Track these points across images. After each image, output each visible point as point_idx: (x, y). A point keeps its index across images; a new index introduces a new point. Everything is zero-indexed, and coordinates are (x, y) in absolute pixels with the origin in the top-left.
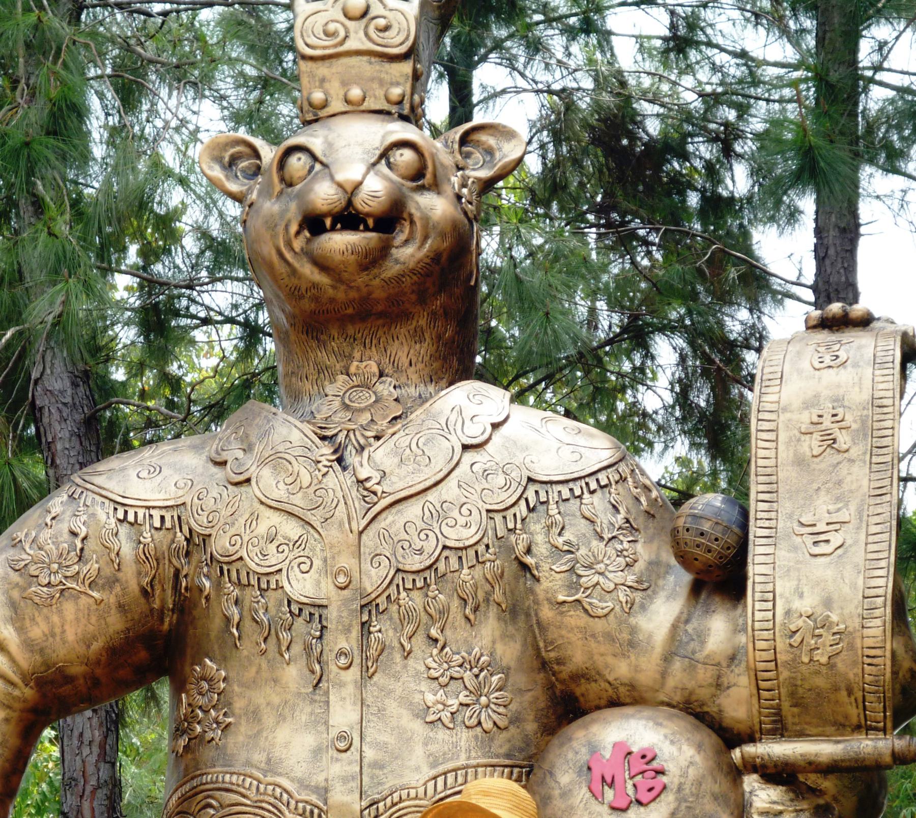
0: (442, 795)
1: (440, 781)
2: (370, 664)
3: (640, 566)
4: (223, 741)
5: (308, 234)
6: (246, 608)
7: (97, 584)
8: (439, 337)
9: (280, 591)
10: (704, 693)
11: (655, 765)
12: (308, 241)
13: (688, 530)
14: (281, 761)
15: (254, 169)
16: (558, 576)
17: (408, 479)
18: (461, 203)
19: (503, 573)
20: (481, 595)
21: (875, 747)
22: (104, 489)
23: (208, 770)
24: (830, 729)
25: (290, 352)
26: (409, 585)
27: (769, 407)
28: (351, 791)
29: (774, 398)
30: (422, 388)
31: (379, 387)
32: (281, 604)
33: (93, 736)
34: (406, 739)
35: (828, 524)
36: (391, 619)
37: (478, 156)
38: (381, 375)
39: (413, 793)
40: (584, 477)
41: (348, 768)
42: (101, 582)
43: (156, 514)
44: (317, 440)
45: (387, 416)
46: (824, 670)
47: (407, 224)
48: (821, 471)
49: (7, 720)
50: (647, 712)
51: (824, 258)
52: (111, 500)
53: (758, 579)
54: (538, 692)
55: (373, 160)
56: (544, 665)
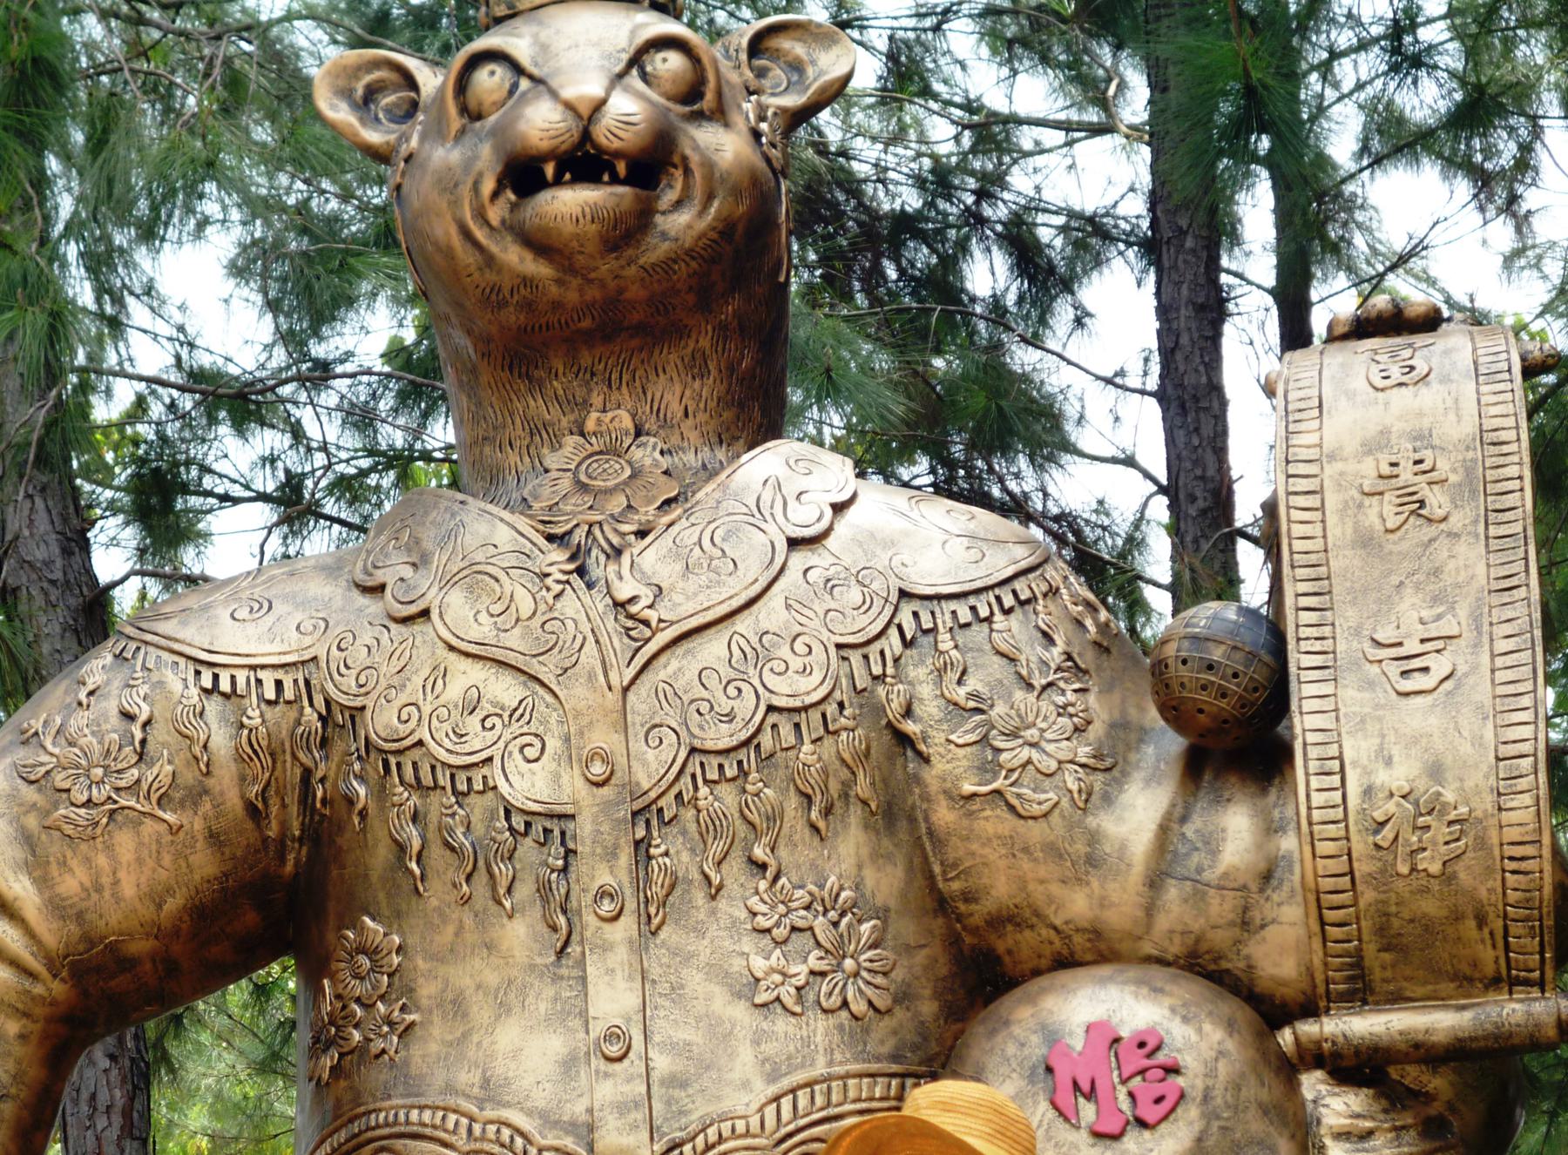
0: (791, 1127)
1: (786, 1103)
2: (652, 910)
3: (1096, 730)
4: (403, 1053)
5: (512, 197)
6: (432, 827)
7: (171, 800)
8: (731, 368)
9: (490, 794)
10: (1220, 938)
11: (1161, 1057)
12: (514, 207)
13: (1184, 662)
14: (507, 1082)
15: (405, 107)
16: (961, 752)
17: (701, 597)
18: (761, 145)
19: (868, 748)
20: (834, 788)
21: (1529, 1014)
22: (176, 640)
23: (378, 1105)
24: (1447, 987)
25: (479, 404)
26: (713, 775)
27: (1304, 454)
28: (634, 1127)
29: (1312, 439)
30: (706, 453)
31: (637, 454)
32: (493, 816)
33: (112, 1097)
34: (721, 1035)
35: (1422, 641)
36: (684, 833)
37: (778, 74)
38: (638, 434)
39: (740, 1126)
40: (992, 587)
41: (626, 1088)
42: (177, 795)
43: (268, 678)
44: (542, 541)
45: (654, 498)
46: (1435, 885)
47: (678, 173)
48: (1404, 556)
49: (22, 1037)
50: (1133, 972)
51: (1173, 350)
52: (189, 658)
53: (1311, 738)
54: (936, 948)
55: (618, 68)
56: (941, 904)
